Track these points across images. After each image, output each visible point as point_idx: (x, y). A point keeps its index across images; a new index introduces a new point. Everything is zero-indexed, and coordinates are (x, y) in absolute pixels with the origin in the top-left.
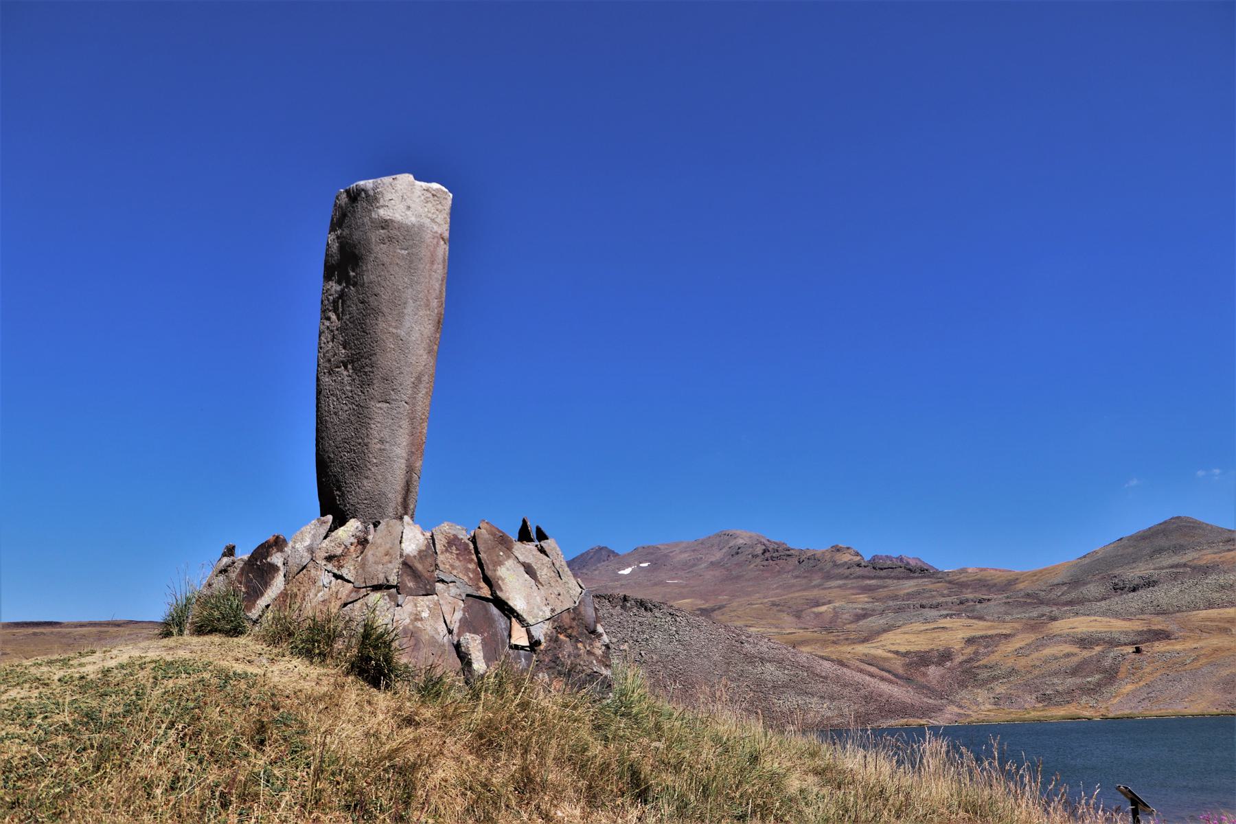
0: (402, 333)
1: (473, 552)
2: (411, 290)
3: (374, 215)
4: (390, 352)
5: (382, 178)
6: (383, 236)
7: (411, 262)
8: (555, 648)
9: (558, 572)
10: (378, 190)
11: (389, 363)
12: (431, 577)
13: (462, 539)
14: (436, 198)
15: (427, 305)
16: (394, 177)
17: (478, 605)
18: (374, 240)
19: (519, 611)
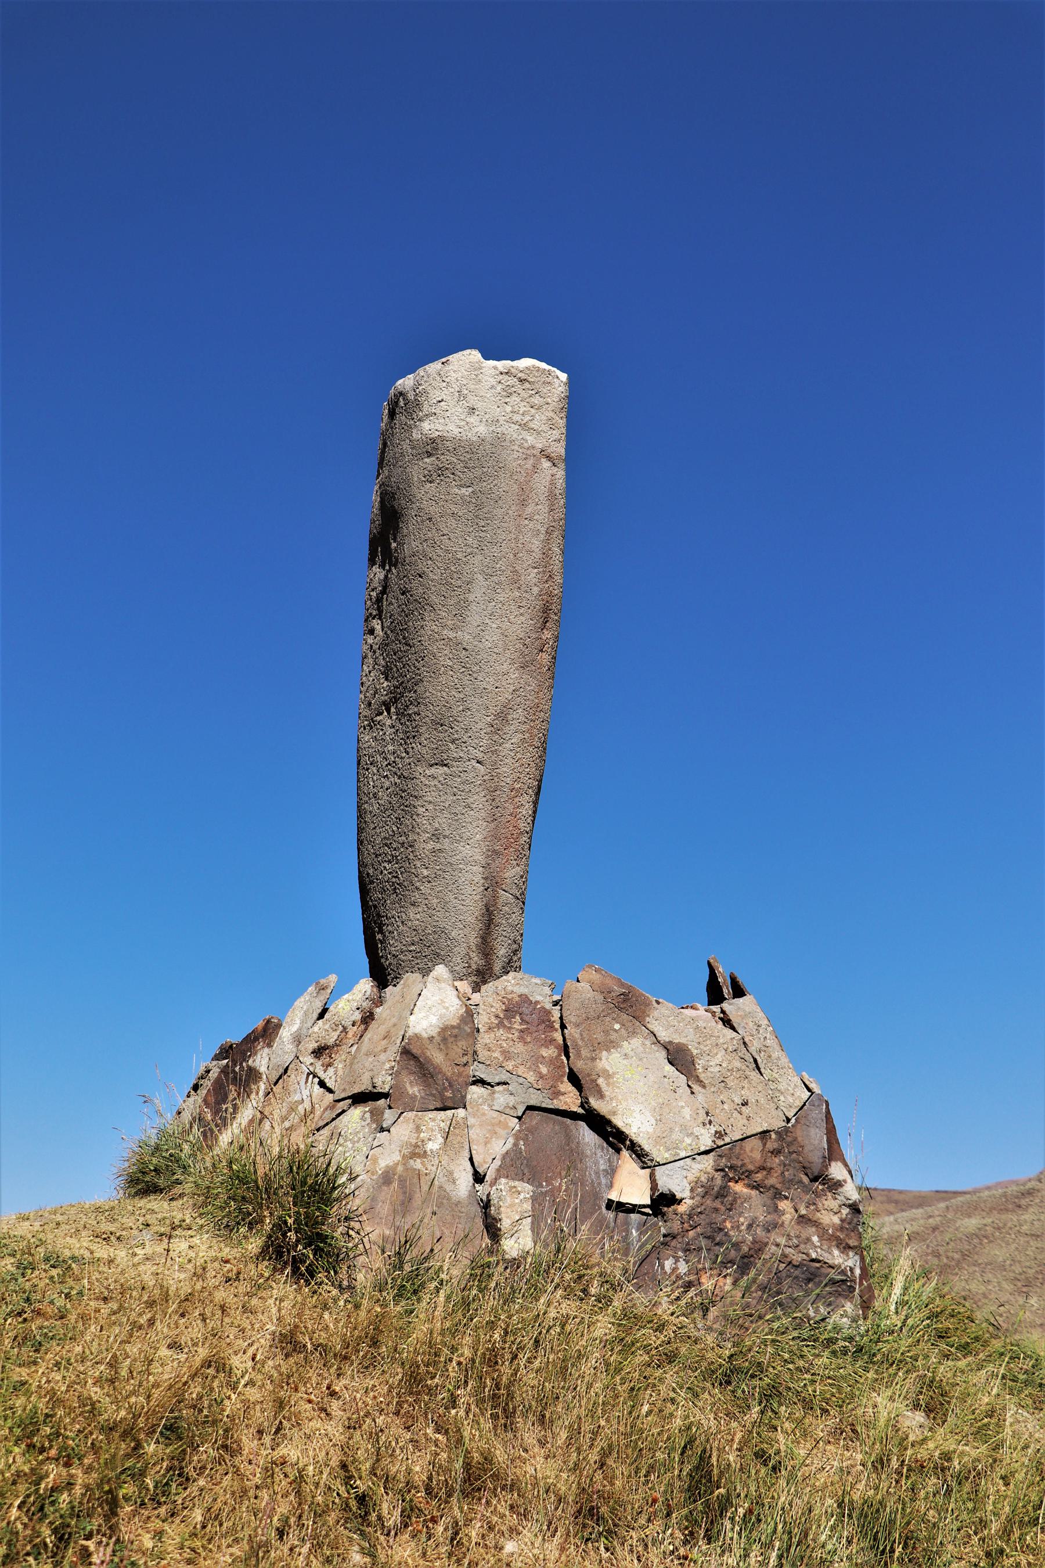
0: (465, 636)
1: (557, 1026)
2: (480, 557)
3: (416, 435)
4: (445, 673)
5: (426, 367)
6: (430, 468)
7: (479, 507)
8: (716, 1210)
9: (755, 1061)
10: (421, 388)
11: (444, 694)
12: (460, 1074)
13: (537, 1002)
14: (527, 385)
15: (515, 581)
16: (444, 360)
17: (551, 1126)
18: (416, 479)
19: (634, 1138)
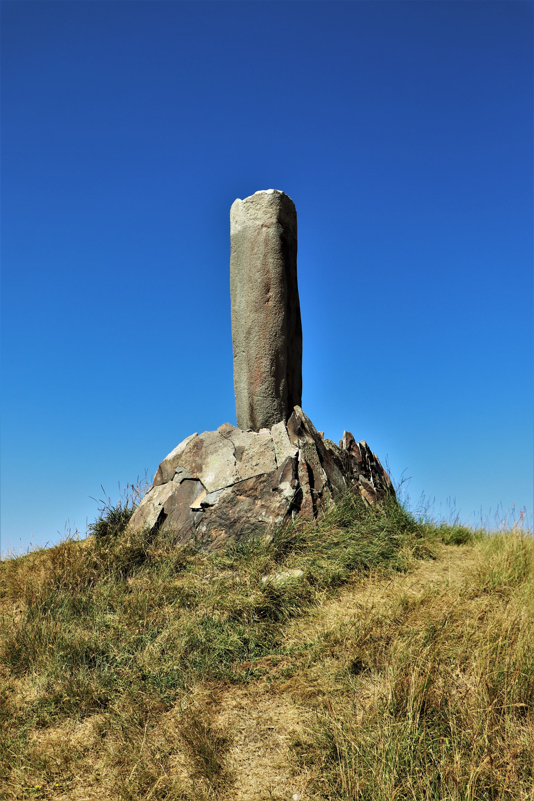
14: (254, 203)
